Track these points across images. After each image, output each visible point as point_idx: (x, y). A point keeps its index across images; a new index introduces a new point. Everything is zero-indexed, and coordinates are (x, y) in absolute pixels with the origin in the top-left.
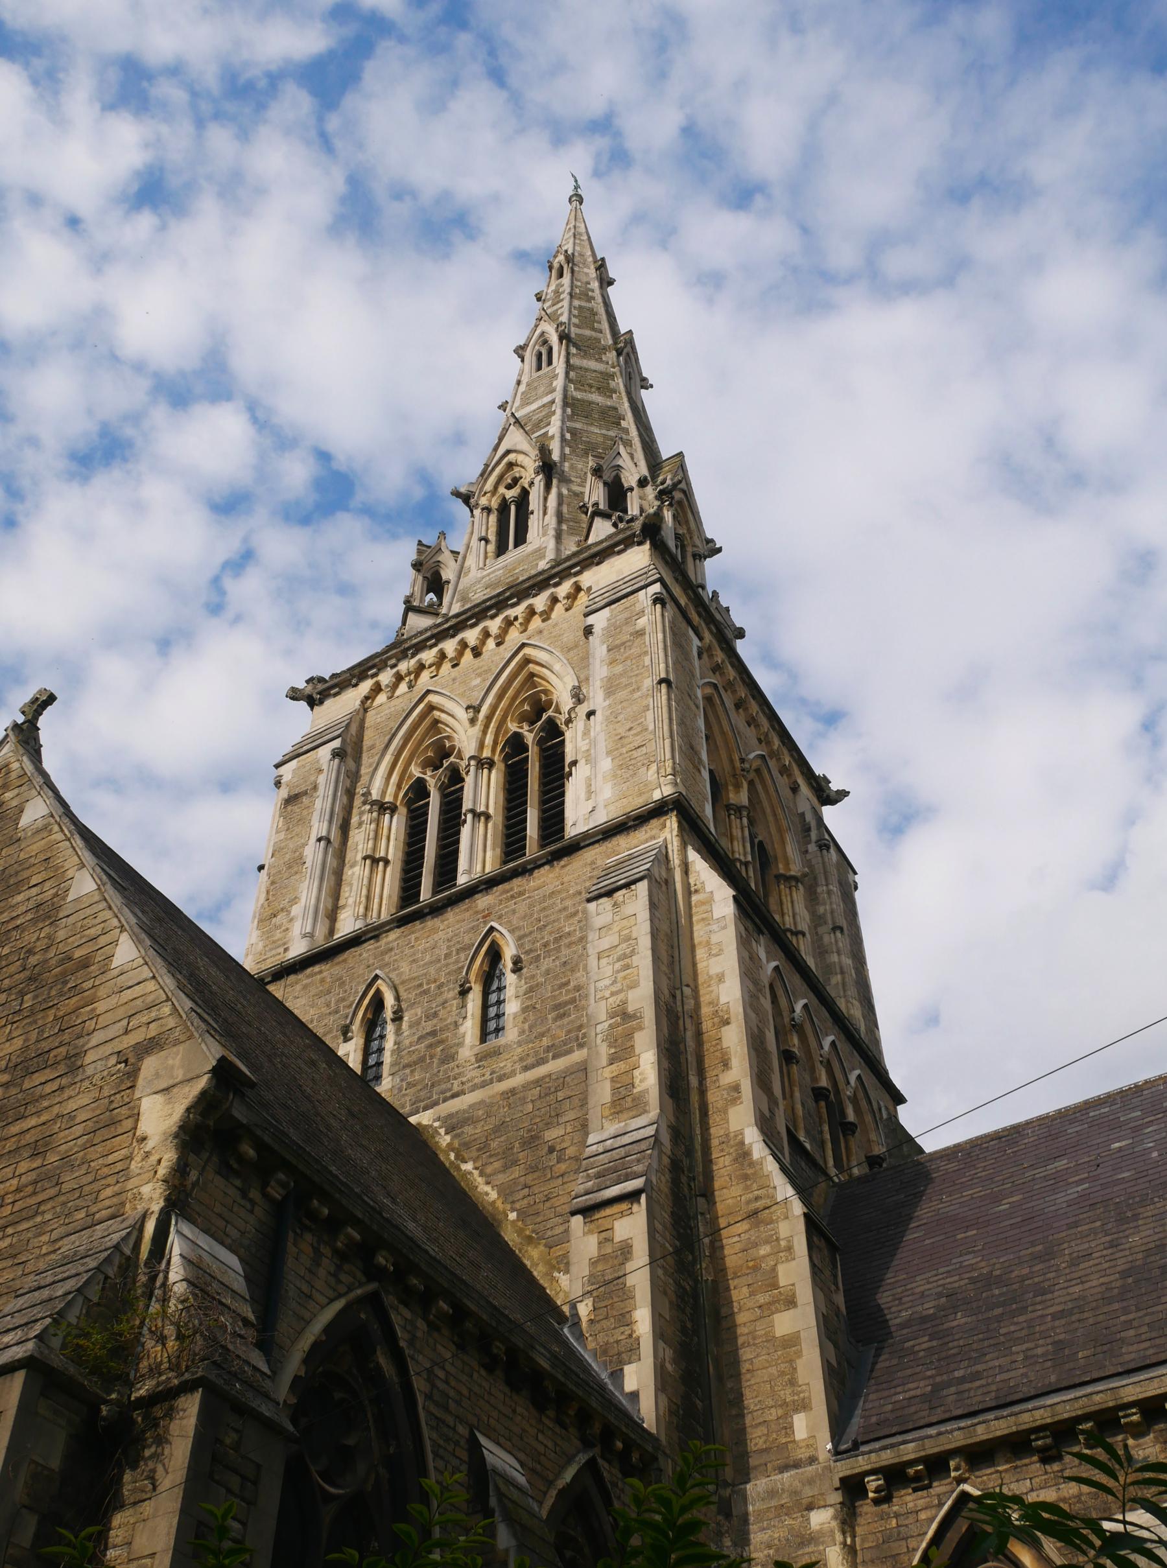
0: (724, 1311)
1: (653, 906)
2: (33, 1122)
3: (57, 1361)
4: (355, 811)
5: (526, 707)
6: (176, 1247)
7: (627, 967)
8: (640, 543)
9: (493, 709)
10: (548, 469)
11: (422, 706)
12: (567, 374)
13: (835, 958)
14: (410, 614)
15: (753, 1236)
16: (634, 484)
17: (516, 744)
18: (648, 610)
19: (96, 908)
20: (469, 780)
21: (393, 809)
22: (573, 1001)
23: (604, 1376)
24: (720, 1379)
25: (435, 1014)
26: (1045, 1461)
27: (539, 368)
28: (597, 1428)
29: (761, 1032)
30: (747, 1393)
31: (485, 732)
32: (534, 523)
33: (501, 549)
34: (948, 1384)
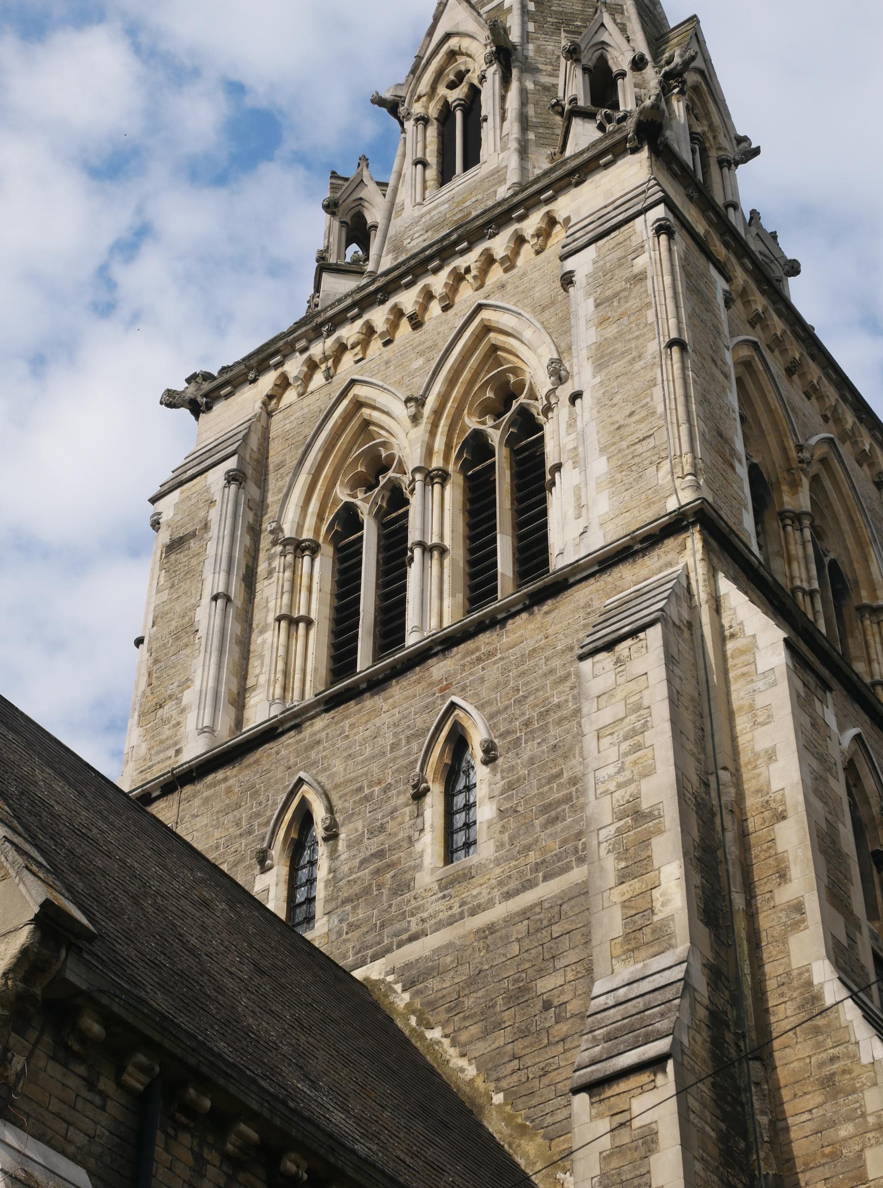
1: (670, 660)
4: (262, 555)
5: (489, 394)
7: (638, 747)
8: (635, 150)
9: (443, 399)
10: (504, 55)
11: (345, 403)
14: (325, 276)
15: (829, 1110)
16: (626, 66)
17: (477, 448)
20: (415, 501)
21: (314, 549)
22: (568, 799)
25: (382, 828)
31: (433, 433)
32: (488, 133)
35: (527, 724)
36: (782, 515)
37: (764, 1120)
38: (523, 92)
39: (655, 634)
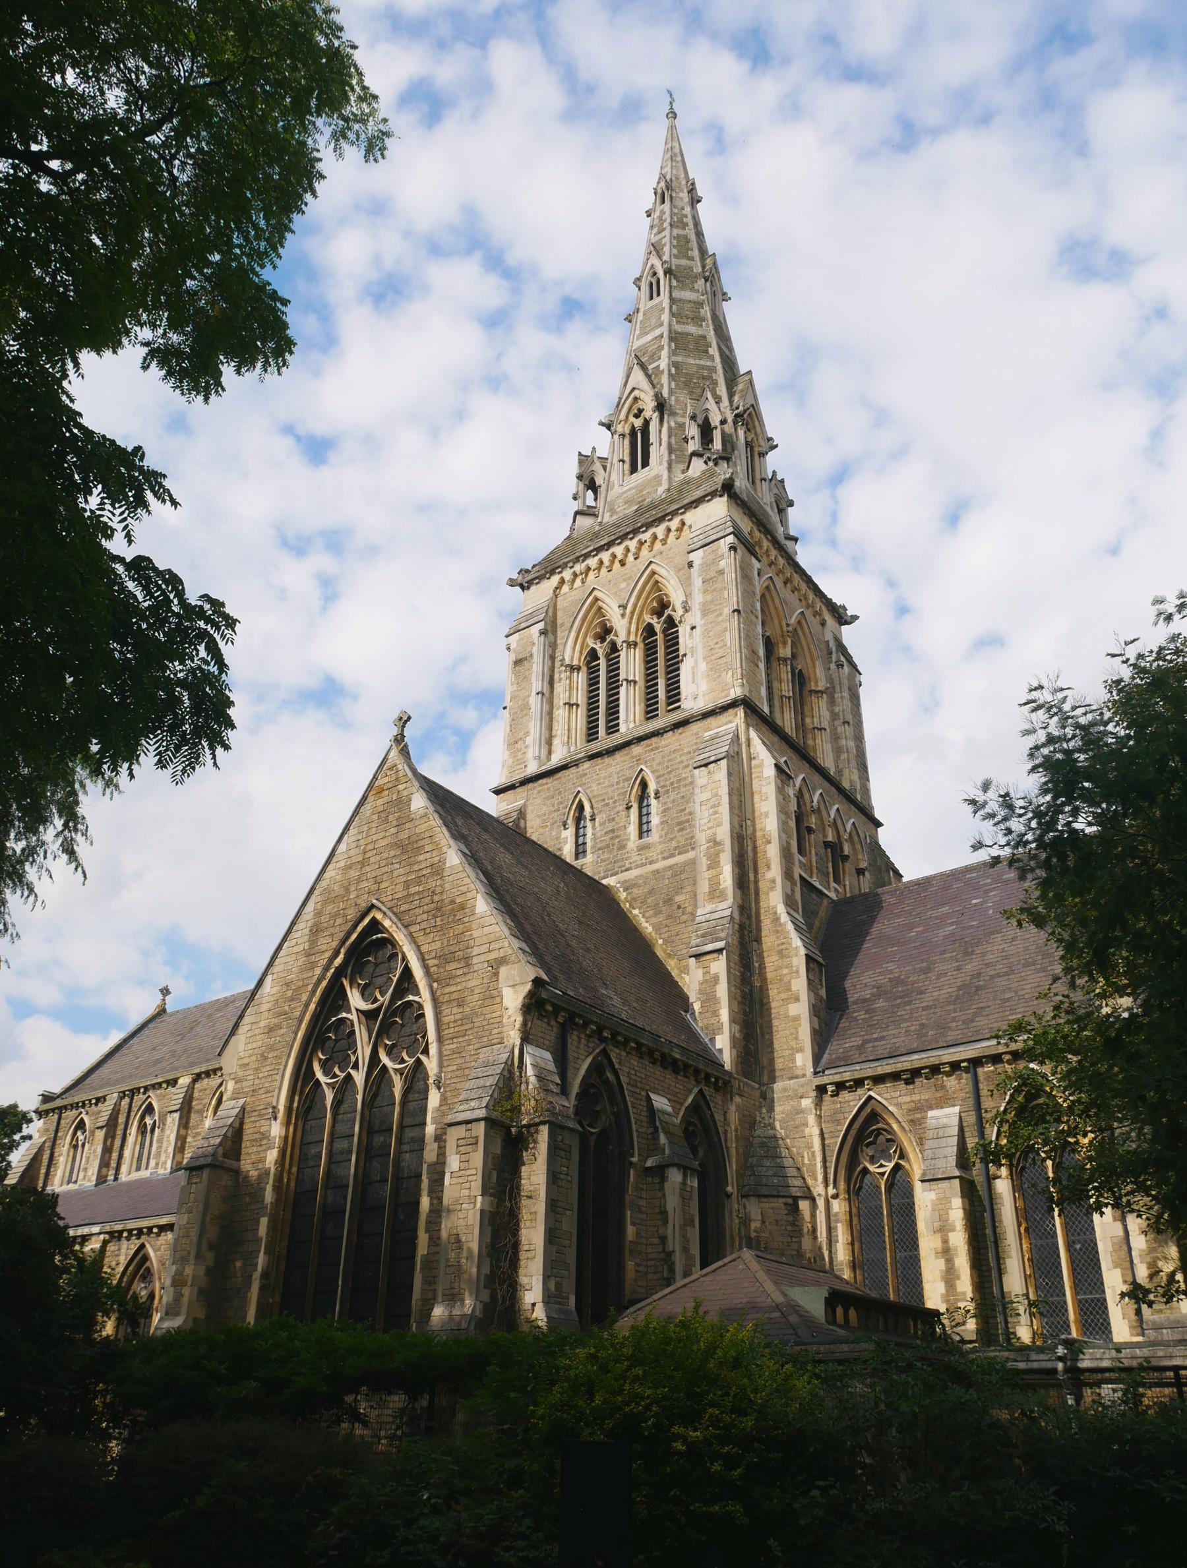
0: (765, 1001)
1: (730, 774)
2: (454, 988)
3: (495, 1115)
4: (556, 670)
5: (655, 604)
6: (528, 1060)
7: (716, 813)
9: (635, 605)
10: (661, 407)
11: (591, 598)
12: (671, 307)
13: (843, 742)
15: (780, 963)
16: (718, 424)
17: (649, 630)
18: (726, 555)
19: (459, 876)
20: (623, 654)
21: (579, 669)
22: (688, 821)
23: (707, 1040)
24: (763, 1035)
25: (613, 819)
26: (907, 1084)
27: (651, 298)
28: (703, 1075)
29: (788, 843)
30: (775, 1041)
31: (630, 623)
32: (653, 450)
33: (634, 470)
34: (870, 1041)
35: (672, 784)
36: (779, 659)
37: (757, 965)
38: (670, 428)
39: (724, 763)
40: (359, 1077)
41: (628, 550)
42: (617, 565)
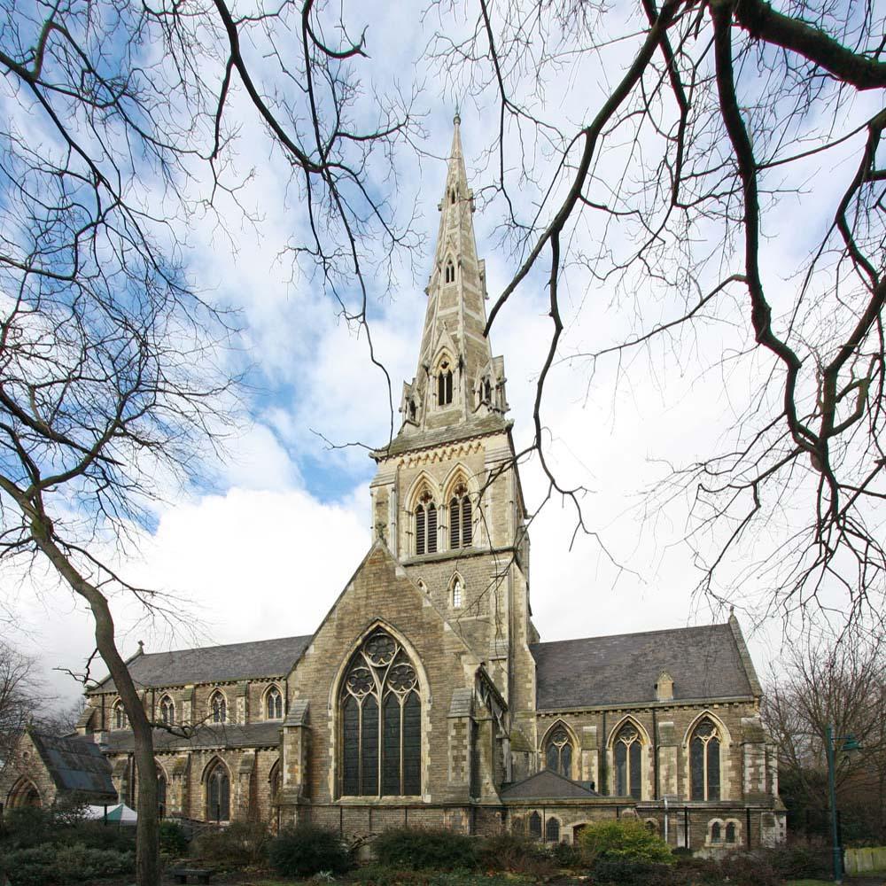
8: (504, 434)
14: (407, 424)
17: (454, 502)
27: (448, 281)
32: (455, 393)
40: (378, 697)
41: (444, 452)
42: (437, 460)
